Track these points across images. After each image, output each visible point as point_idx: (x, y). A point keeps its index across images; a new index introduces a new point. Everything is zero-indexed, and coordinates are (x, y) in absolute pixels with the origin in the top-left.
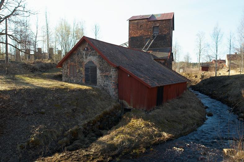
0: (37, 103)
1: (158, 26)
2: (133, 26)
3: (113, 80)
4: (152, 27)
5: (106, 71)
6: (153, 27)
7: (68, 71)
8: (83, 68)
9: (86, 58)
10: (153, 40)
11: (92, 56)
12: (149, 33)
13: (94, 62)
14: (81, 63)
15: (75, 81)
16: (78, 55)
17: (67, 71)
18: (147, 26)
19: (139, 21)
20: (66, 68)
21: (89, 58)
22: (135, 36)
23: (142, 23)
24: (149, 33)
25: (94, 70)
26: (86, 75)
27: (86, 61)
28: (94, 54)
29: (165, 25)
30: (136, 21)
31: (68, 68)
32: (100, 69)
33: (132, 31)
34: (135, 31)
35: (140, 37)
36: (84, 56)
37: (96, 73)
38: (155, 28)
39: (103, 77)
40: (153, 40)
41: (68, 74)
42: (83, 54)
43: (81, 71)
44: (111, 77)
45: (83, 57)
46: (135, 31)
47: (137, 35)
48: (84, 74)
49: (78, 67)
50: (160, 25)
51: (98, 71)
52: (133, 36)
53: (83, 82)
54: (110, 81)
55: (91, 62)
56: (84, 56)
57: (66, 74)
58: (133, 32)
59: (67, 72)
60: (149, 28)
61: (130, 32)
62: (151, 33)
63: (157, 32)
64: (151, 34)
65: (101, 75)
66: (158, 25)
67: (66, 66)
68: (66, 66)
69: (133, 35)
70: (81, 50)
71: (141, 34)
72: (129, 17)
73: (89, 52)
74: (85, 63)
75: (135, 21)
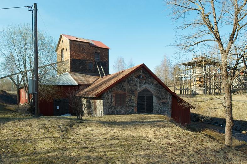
0: (104, 147)
1: (99, 53)
2: (74, 47)
3: (170, 106)
5: (163, 99)
6: (95, 53)
7: (113, 101)
8: (135, 97)
9: (140, 86)
10: (102, 67)
11: (147, 85)
12: (92, 58)
13: (151, 90)
14: (133, 92)
15: (123, 112)
16: (129, 82)
17: (111, 100)
18: (89, 51)
20: (110, 98)
21: (144, 86)
23: (84, 47)
24: (92, 58)
25: (150, 98)
26: (138, 104)
27: (139, 89)
28: (150, 82)
30: (78, 43)
31: (112, 97)
32: (157, 97)
33: (74, 52)
34: (77, 53)
35: (83, 60)
36: (138, 84)
37: (153, 101)
38: (96, 54)
39: (160, 104)
40: (102, 67)
41: (114, 105)
42: (137, 82)
43: (133, 100)
44: (168, 103)
45: (136, 85)
46: (77, 53)
47: (79, 58)
49: (129, 96)
51: (155, 100)
52: (74, 58)
53: (135, 111)
54: (167, 107)
55: (146, 90)
56: (138, 84)
57: (110, 105)
59: (111, 103)
60: (91, 53)
61: (72, 53)
62: (93, 58)
64: (93, 59)
65: (158, 102)
66: (99, 52)
67: (110, 95)
68: (110, 95)
69: (75, 57)
70: (134, 77)
71: (83, 57)
73: (144, 80)
74: (139, 92)
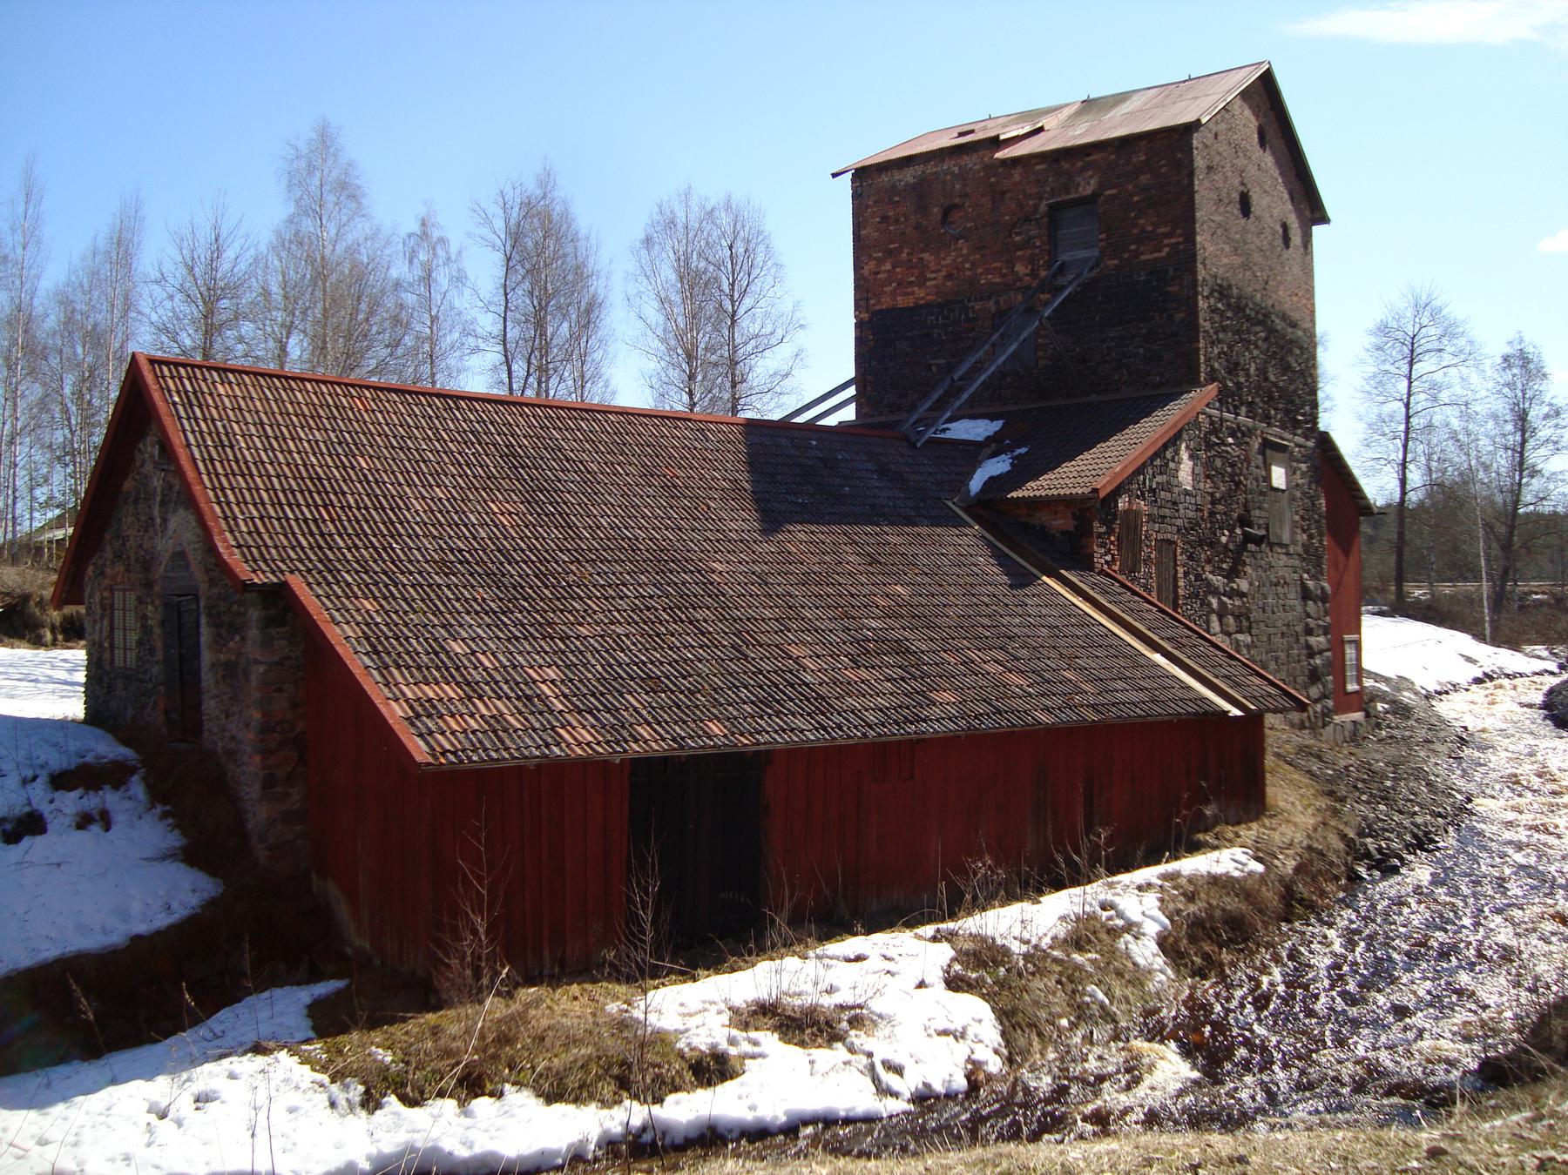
1: (1092, 199)
4: (1043, 207)
12: (1020, 268)
19: (931, 168)
22: (909, 302)
24: (1020, 268)
27: (164, 546)
29: (1144, 179)
33: (880, 261)
48: (159, 655)
50: (1102, 186)
52: (886, 302)
58: (888, 266)
63: (1083, 254)
66: (1089, 191)
71: (949, 276)
72: (918, 112)
75: (897, 175)
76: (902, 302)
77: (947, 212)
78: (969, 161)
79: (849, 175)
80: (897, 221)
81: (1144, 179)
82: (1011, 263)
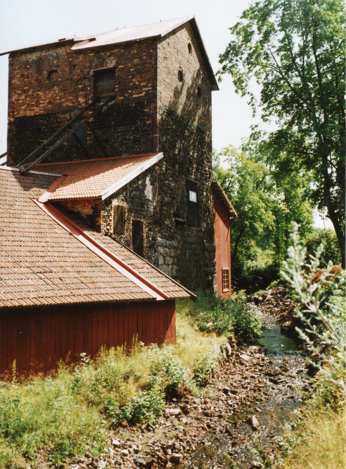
4: (91, 73)
19: (44, 54)
29: (136, 61)
30: (34, 57)
33: (20, 95)
47: (36, 109)
50: (118, 64)
52: (21, 114)
58: (23, 97)
66: (112, 66)
71: (50, 103)
76: (29, 113)
77: (50, 73)
78: (61, 51)
79: (8, 55)
80: (28, 77)
81: (136, 61)
82: (77, 97)
